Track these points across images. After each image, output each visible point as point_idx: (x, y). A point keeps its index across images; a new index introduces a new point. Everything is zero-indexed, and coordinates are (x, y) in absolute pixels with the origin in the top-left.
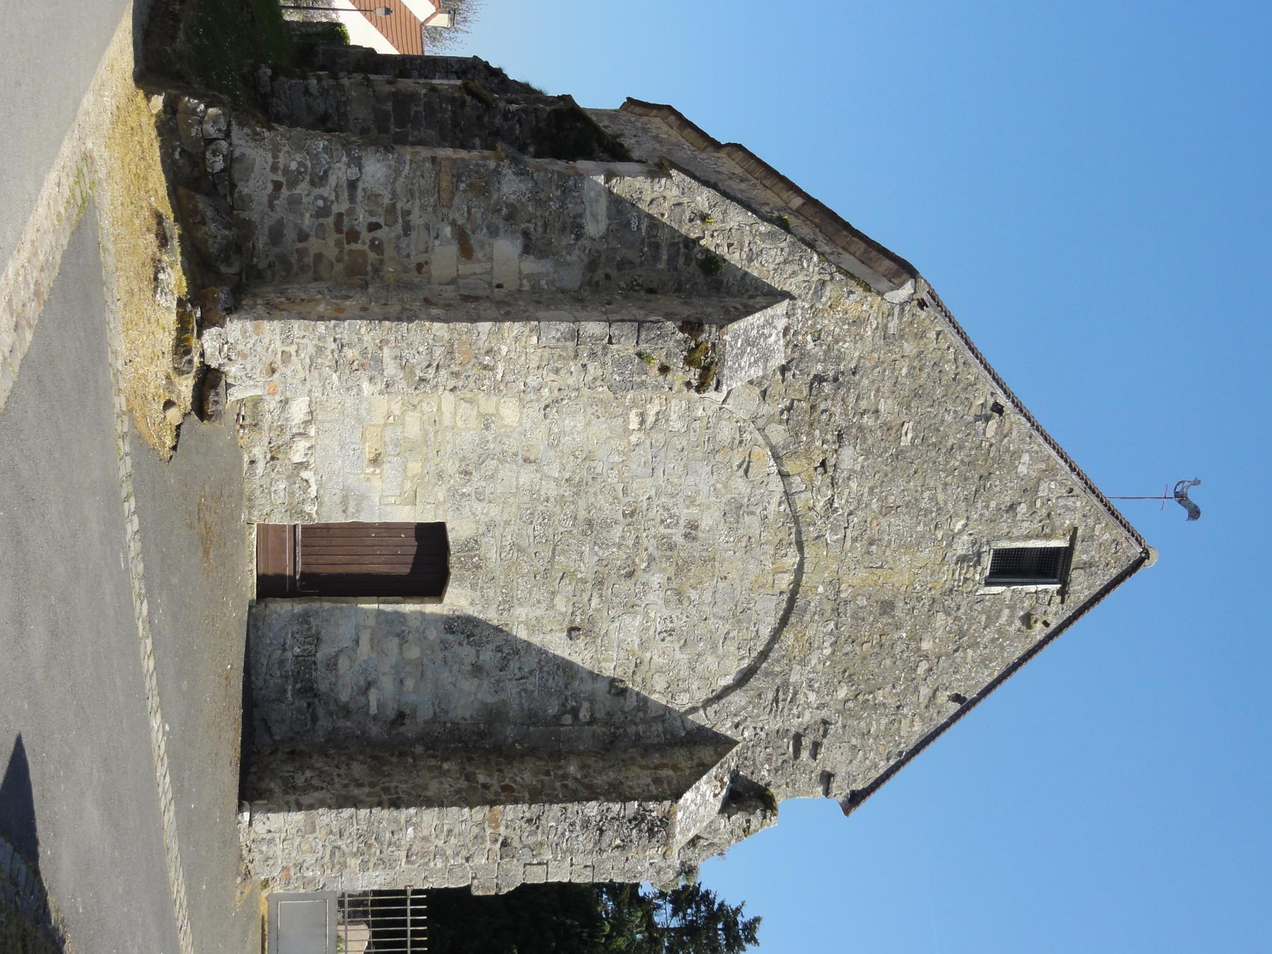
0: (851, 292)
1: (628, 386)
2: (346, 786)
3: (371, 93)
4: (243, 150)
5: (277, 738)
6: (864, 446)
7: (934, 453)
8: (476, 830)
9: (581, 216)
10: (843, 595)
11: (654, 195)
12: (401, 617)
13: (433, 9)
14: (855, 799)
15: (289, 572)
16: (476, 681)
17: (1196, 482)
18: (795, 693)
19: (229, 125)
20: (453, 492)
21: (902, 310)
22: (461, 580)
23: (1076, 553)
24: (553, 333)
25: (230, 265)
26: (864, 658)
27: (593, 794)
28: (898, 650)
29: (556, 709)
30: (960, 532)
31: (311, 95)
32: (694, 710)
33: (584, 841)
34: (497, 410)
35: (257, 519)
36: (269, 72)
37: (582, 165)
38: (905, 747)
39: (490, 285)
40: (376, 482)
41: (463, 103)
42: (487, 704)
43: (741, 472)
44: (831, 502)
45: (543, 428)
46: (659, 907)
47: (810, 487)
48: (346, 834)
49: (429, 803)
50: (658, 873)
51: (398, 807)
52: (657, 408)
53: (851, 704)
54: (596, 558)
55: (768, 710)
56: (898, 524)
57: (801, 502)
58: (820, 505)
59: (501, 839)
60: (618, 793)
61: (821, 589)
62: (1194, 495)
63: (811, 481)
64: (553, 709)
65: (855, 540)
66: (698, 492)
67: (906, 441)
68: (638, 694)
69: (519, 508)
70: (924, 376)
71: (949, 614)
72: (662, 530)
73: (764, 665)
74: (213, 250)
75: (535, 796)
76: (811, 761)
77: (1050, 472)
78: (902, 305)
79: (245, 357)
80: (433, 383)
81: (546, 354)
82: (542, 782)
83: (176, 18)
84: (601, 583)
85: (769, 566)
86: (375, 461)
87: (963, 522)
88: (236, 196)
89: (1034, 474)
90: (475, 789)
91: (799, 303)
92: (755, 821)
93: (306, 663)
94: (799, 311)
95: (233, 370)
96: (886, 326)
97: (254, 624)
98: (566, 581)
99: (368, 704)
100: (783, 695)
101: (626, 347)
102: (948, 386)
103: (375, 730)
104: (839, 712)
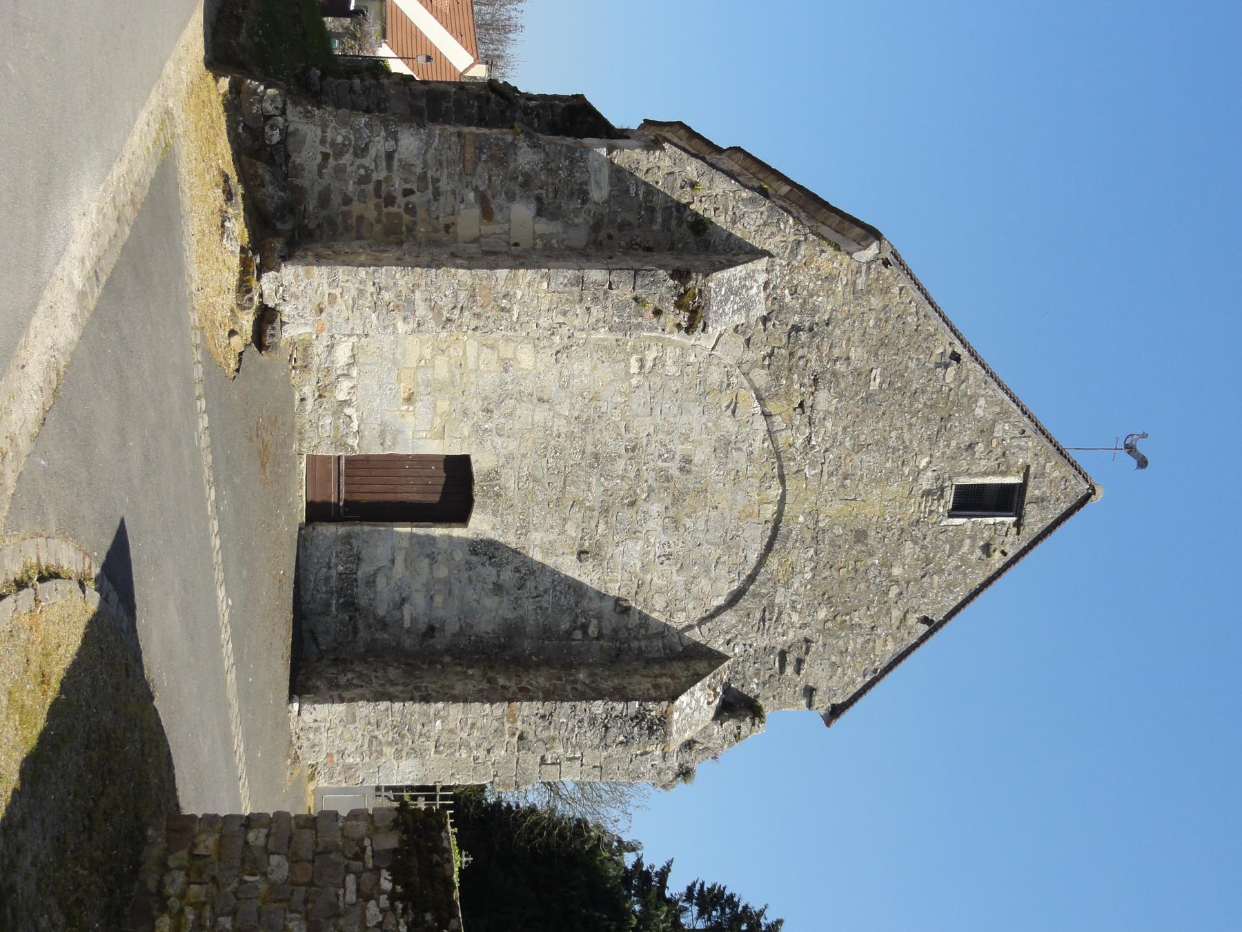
0: (823, 251)
1: (626, 328)
2: (382, 685)
3: (407, 91)
4: (296, 125)
5: (323, 648)
6: (838, 390)
7: (899, 397)
8: (496, 724)
9: (586, 183)
10: (821, 525)
11: (650, 165)
12: (432, 540)
13: (471, 60)
14: (835, 712)
15: (333, 499)
16: (497, 599)
17: (1144, 436)
18: (780, 613)
19: (285, 104)
20: (476, 428)
21: (869, 268)
22: (484, 506)
23: (1029, 489)
24: (561, 279)
25: (284, 222)
26: (841, 582)
27: (599, 695)
28: (871, 575)
29: (568, 625)
30: (925, 468)
31: (355, 93)
32: (690, 627)
33: (591, 736)
34: (515, 353)
35: (306, 451)
36: (319, 73)
37: (587, 141)
38: (879, 665)
39: (508, 243)
40: (410, 419)
41: (488, 100)
42: (506, 620)
43: (729, 412)
44: (809, 439)
45: (555, 371)
46: (686, 909)
47: (790, 426)
48: (383, 725)
49: (455, 699)
50: (659, 774)
51: (427, 702)
52: (654, 355)
53: (830, 625)
54: (602, 489)
55: (756, 628)
56: (868, 460)
57: (782, 439)
58: (799, 442)
59: (518, 733)
60: (624, 696)
61: (801, 519)
62: (1142, 447)
63: (791, 420)
64: (565, 626)
65: (831, 474)
66: (691, 430)
67: (874, 386)
68: (640, 612)
69: (534, 443)
70: (890, 327)
71: (916, 543)
72: (660, 464)
73: (752, 587)
74: (271, 208)
75: (547, 696)
76: (795, 676)
77: (1004, 414)
78: (869, 264)
79: (297, 298)
80: (458, 322)
81: (555, 298)
82: (555, 685)
83: (239, 20)
84: (607, 511)
85: (755, 497)
86: (409, 399)
87: (927, 459)
88: (290, 165)
89: (991, 417)
90: (496, 689)
91: (777, 260)
92: (745, 726)
93: (348, 579)
94: (778, 268)
95: (287, 309)
96: (854, 283)
97: (303, 542)
98: (576, 508)
99: (402, 619)
100: (769, 615)
101: (624, 292)
102: (911, 336)
103: (408, 642)
104: (819, 631)
